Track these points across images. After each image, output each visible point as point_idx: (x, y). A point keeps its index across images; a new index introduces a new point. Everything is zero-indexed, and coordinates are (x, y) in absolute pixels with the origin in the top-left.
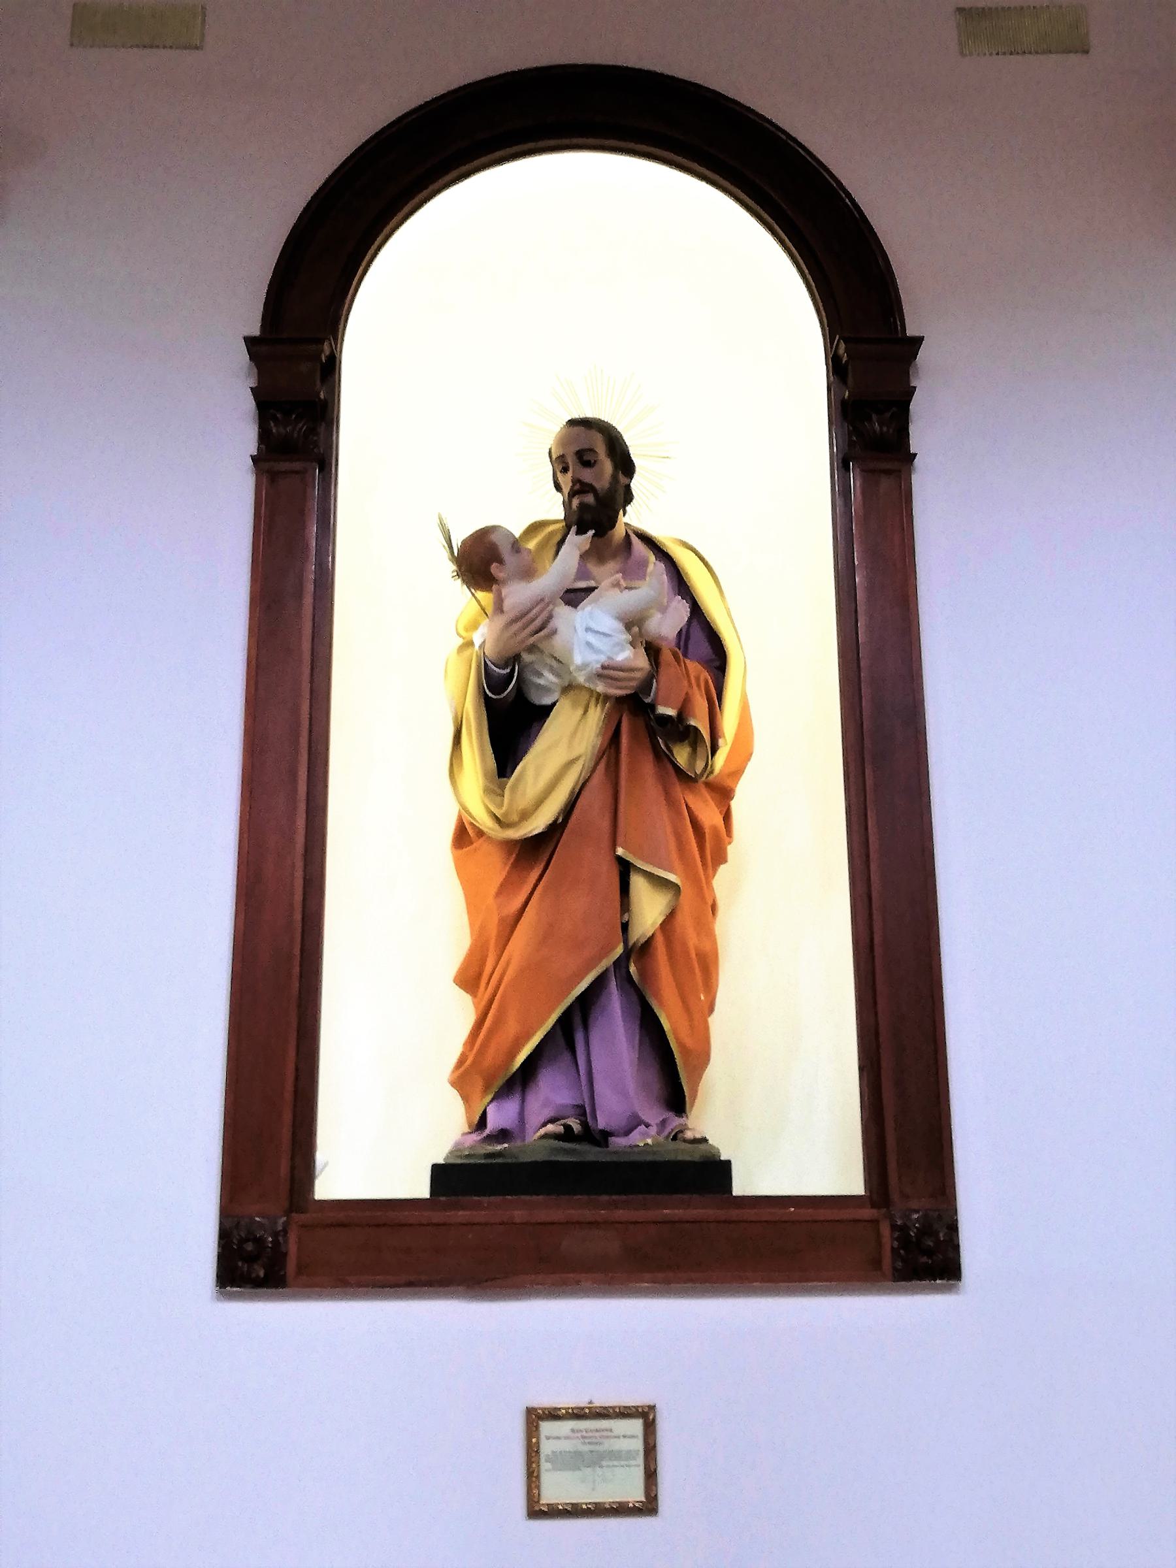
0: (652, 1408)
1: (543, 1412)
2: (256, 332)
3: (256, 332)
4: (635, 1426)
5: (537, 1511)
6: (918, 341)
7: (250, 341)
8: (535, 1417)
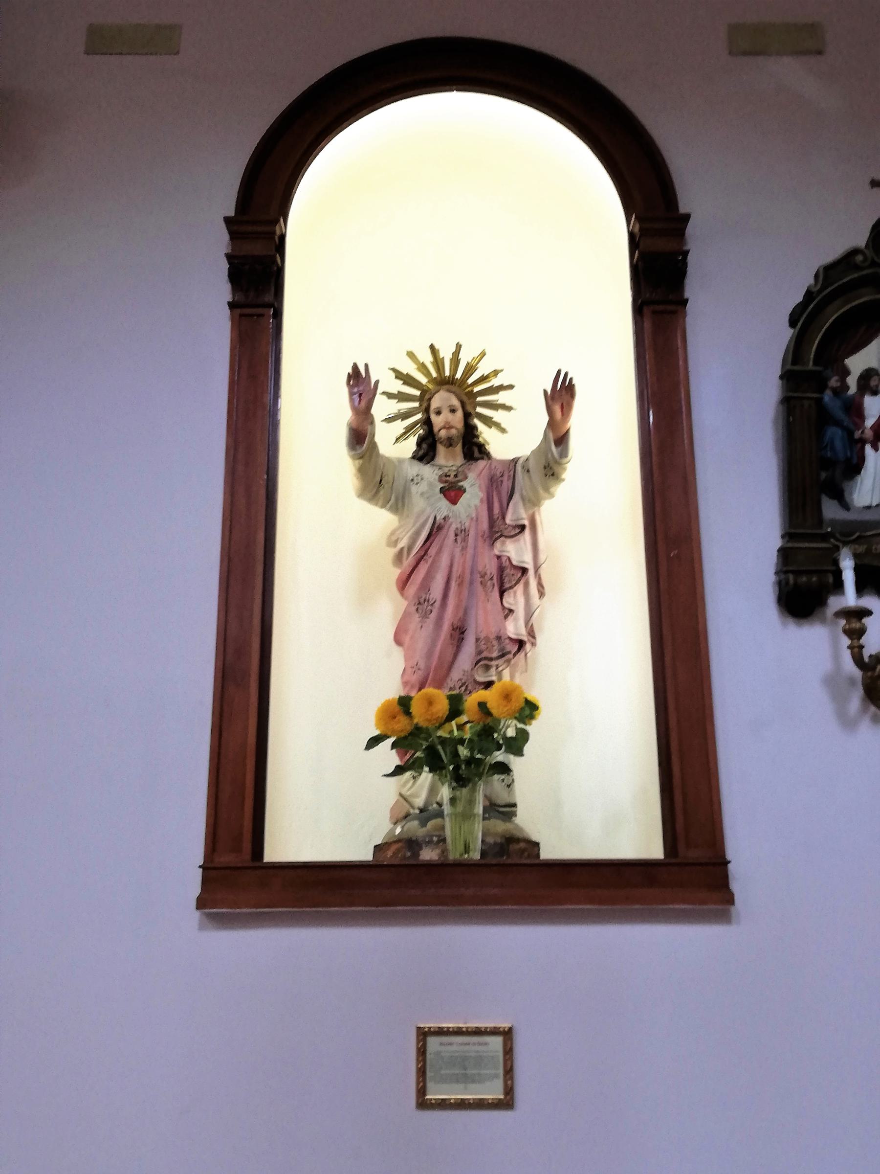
2: (232, 213)
3: (232, 213)
4: (497, 1042)
5: (423, 1104)
6: (687, 218)
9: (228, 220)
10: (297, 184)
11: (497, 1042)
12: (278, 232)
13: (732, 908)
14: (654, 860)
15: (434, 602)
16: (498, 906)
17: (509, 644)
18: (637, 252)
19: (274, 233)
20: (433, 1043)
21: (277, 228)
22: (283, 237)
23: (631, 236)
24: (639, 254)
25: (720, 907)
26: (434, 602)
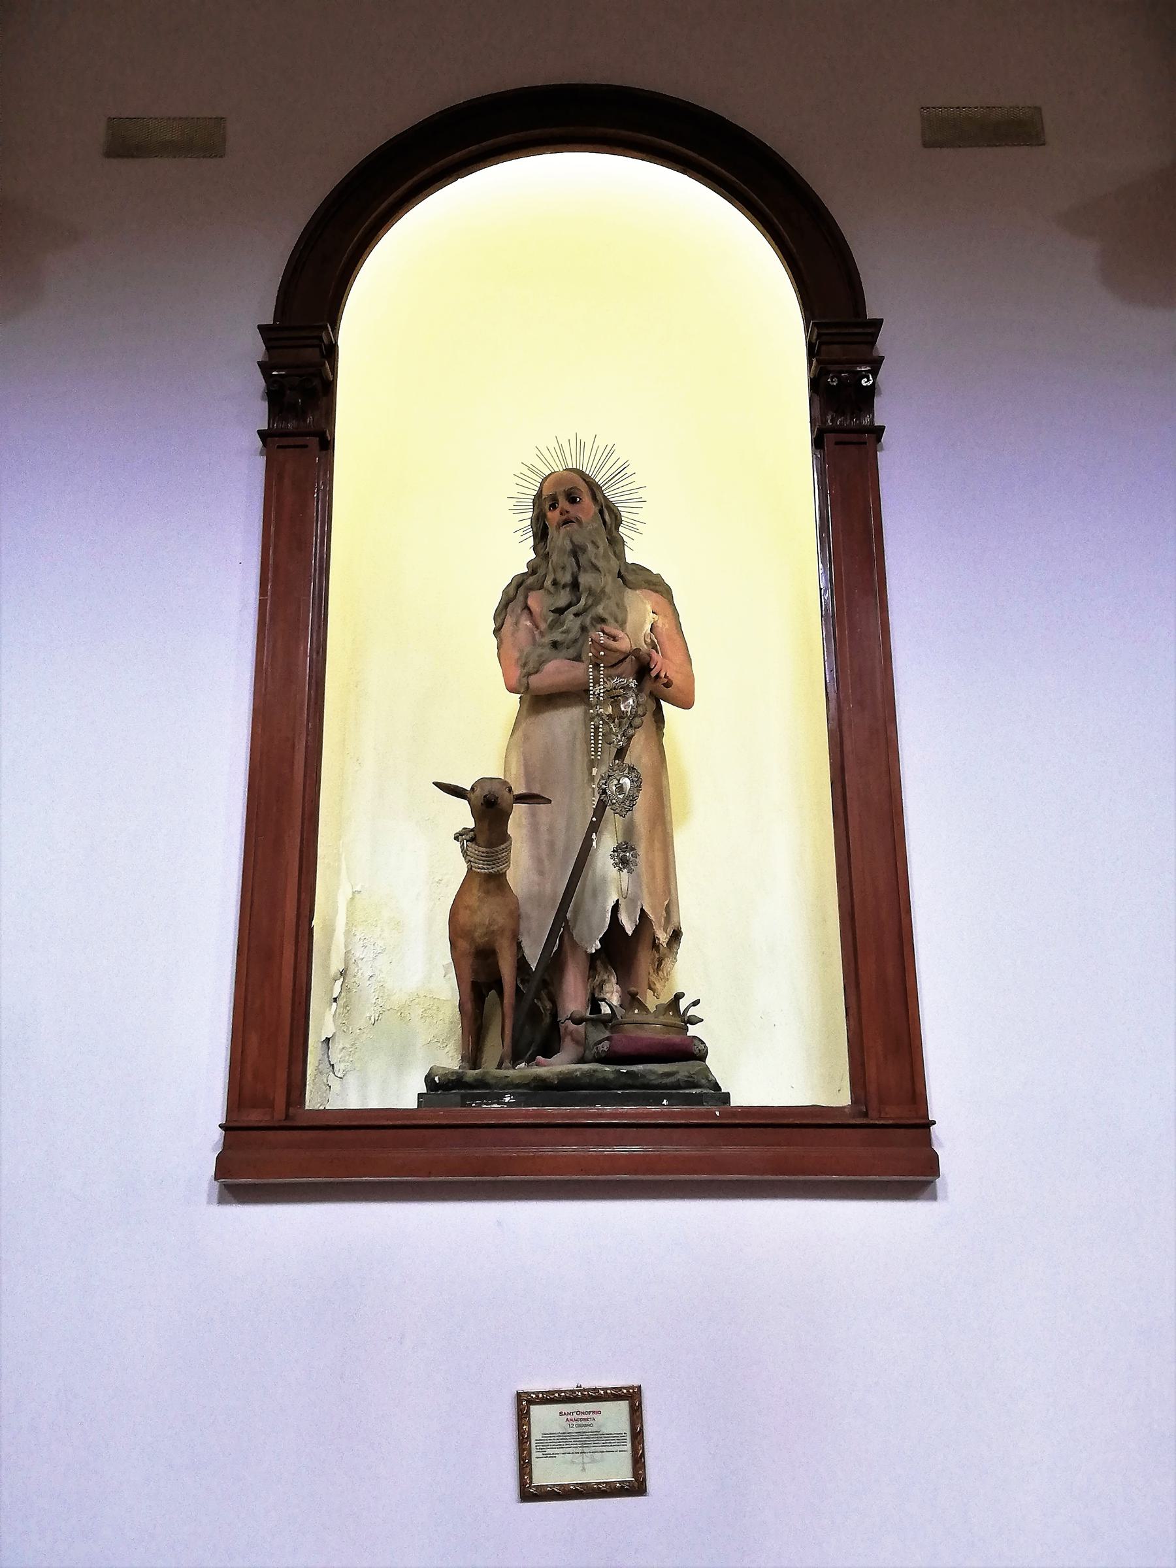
0: (519, 1395)
2: (264, 426)
5: (529, 1493)
6: (878, 323)
7: (262, 329)
8: (525, 1402)
9: (262, 329)
20: (618, 1469)
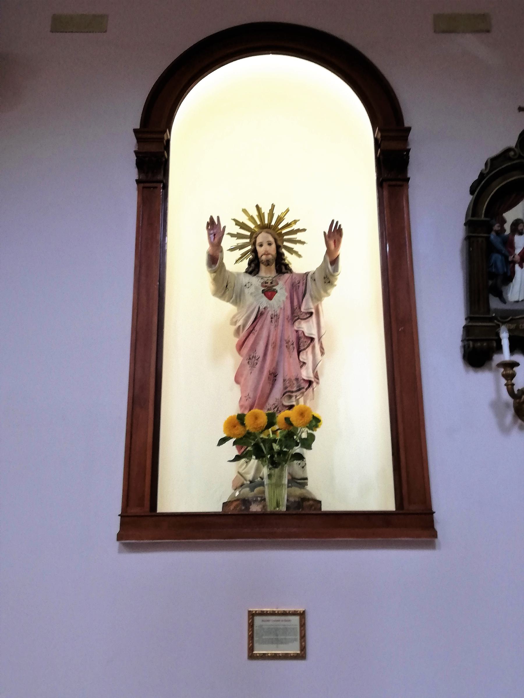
1: (251, 619)
2: (138, 127)
3: (138, 127)
4: (296, 620)
5: (252, 656)
6: (409, 129)
9: (135, 131)
10: (177, 110)
11: (296, 620)
12: (166, 138)
13: (436, 540)
14: (390, 511)
15: (259, 358)
16: (296, 539)
17: (303, 383)
18: (379, 150)
19: (163, 138)
21: (165, 135)
22: (168, 141)
23: (376, 140)
24: (381, 151)
25: (429, 539)
26: (259, 358)
